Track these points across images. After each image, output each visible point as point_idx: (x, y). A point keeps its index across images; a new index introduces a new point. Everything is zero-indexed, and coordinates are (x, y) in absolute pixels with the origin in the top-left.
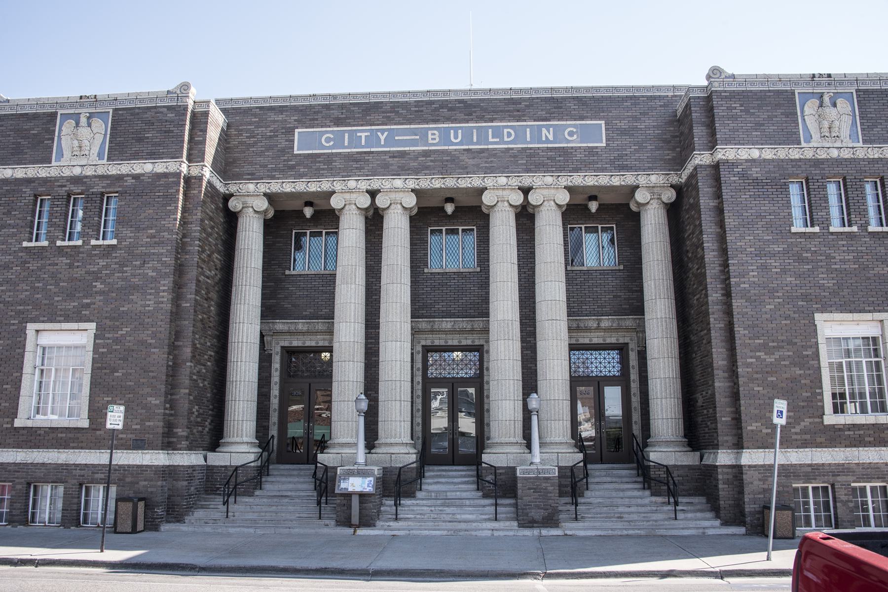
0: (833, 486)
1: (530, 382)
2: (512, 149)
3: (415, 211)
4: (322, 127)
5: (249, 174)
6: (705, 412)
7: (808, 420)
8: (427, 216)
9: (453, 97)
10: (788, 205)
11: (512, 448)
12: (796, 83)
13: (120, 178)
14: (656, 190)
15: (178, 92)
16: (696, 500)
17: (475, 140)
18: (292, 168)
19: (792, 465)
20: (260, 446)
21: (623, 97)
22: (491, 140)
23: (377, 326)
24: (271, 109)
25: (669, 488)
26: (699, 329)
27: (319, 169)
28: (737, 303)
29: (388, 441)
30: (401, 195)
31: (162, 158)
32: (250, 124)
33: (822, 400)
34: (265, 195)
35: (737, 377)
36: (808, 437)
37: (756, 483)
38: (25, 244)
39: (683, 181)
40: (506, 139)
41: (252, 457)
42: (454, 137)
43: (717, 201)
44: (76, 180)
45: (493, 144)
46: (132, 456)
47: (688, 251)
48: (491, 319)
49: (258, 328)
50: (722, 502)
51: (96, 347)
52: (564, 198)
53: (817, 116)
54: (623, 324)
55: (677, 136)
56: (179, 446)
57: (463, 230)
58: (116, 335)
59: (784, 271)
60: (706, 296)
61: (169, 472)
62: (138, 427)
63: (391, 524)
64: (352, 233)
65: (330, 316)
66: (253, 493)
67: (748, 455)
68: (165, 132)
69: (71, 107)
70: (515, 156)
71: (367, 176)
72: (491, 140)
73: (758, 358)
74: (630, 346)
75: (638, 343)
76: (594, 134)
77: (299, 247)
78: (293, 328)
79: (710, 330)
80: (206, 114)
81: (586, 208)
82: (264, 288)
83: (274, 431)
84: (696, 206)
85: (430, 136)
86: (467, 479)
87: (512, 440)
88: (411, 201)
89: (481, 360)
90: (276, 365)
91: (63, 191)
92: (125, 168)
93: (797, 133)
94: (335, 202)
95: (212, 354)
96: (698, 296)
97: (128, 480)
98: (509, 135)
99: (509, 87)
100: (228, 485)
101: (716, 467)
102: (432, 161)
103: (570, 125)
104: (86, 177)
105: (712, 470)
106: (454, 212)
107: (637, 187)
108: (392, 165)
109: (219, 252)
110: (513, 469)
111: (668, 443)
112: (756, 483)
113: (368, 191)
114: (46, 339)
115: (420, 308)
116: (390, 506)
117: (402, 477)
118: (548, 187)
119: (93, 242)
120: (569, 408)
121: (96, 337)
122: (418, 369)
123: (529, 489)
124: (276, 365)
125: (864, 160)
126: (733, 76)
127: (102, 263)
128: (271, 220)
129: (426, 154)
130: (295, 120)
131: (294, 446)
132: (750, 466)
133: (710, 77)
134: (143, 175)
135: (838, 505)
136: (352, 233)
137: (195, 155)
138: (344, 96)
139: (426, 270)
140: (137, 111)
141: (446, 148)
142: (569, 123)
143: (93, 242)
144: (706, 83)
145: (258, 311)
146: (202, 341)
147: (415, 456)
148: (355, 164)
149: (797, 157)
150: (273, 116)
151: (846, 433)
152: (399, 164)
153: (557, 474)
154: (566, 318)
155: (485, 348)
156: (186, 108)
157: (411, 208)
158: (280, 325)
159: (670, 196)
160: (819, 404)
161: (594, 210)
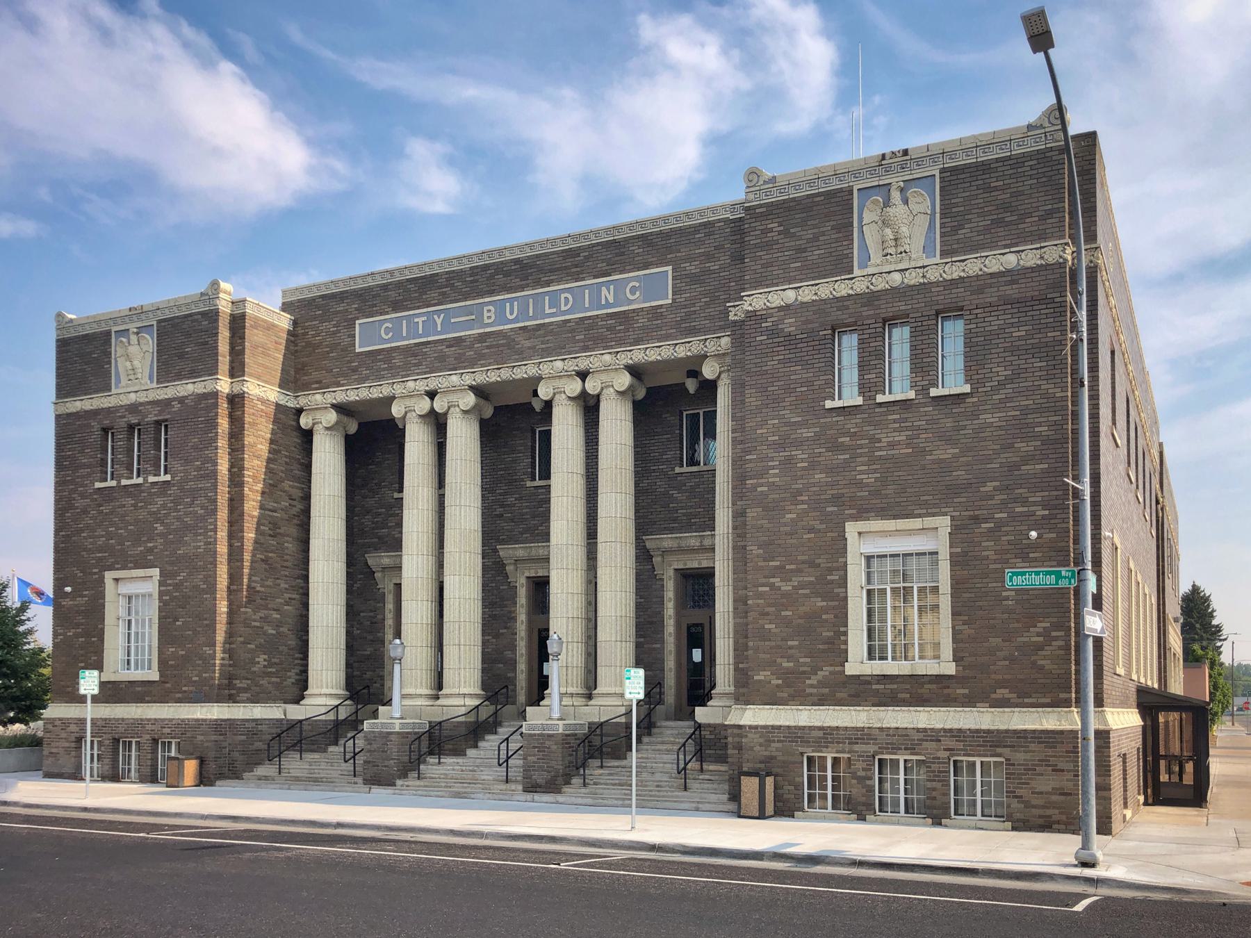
2: (569, 321)
4: (381, 314)
5: (317, 382)
9: (508, 256)
13: (167, 403)
18: (354, 370)
21: (694, 226)
22: (548, 311)
24: (333, 296)
34: (471, 388)
37: (757, 748)
38: (98, 485)
40: (563, 308)
42: (500, 313)
44: (134, 408)
45: (551, 316)
51: (161, 594)
59: (813, 465)
61: (220, 726)
69: (124, 323)
72: (548, 311)
73: (772, 586)
85: (486, 314)
91: (122, 423)
92: (972, 266)
94: (397, 410)
97: (188, 735)
102: (488, 347)
103: (632, 278)
104: (141, 404)
106: (697, 391)
112: (757, 748)
114: (125, 589)
119: (152, 479)
121: (161, 584)
125: (937, 284)
126: (773, 180)
127: (160, 501)
129: (482, 338)
132: (751, 727)
134: (186, 397)
141: (501, 328)
142: (631, 274)
143: (152, 479)
146: (269, 583)
148: (415, 359)
149: (844, 293)
158: (667, 541)
160: (843, 647)
161: (692, 391)
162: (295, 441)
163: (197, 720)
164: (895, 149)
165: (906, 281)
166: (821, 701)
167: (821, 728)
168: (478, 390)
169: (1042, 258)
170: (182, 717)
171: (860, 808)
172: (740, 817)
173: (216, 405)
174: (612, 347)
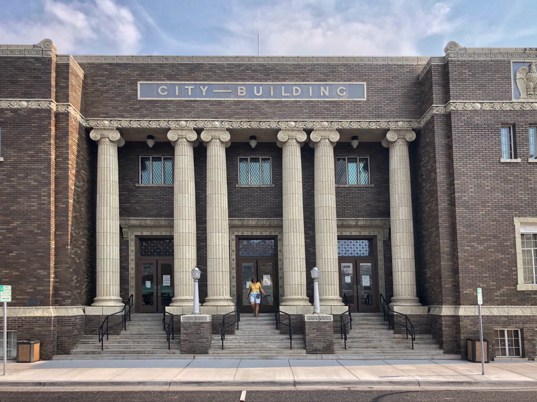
0: (522, 330)
1: (311, 261)
3: (229, 145)
4: (158, 80)
5: (104, 114)
6: (432, 281)
7: (506, 288)
8: (240, 149)
9: (255, 62)
10: (499, 143)
11: (300, 302)
12: (512, 54)
14: (401, 132)
15: (43, 47)
16: (425, 336)
17: (272, 94)
19: (494, 316)
20: (123, 302)
22: (284, 94)
23: (205, 222)
24: (118, 65)
25: (407, 329)
26: (430, 227)
27: (157, 112)
28: (459, 210)
29: (215, 297)
30: (219, 133)
31: (34, 98)
32: (103, 76)
33: (516, 275)
34: (118, 129)
35: (457, 259)
36: (506, 298)
37: (469, 327)
39: (421, 126)
40: (294, 94)
41: (118, 310)
42: (258, 92)
43: (448, 140)
46: (28, 310)
47: (422, 175)
48: (392, 218)
49: (118, 223)
50: (444, 339)
52: (336, 137)
53: (525, 79)
54: (272, 223)
55: (418, 94)
56: (64, 303)
57: (263, 159)
58: (9, 227)
60: (437, 205)
62: (32, 290)
63: (219, 352)
64: (185, 158)
65: (171, 214)
66: (120, 332)
67: (463, 309)
68: (35, 77)
70: (301, 107)
71: (194, 118)
73: (472, 247)
74: (378, 238)
75: (384, 235)
76: (356, 92)
77: (144, 168)
78: (143, 223)
79: (438, 227)
80: (67, 66)
81: (349, 145)
82: (120, 195)
83: (132, 292)
84: (432, 144)
85: (239, 91)
86: (266, 318)
87: (300, 297)
88: (227, 137)
89: (276, 245)
90: (132, 247)
93: (509, 92)
94: (171, 136)
95: (85, 240)
96: (430, 205)
98: (297, 91)
99: (297, 55)
100: (104, 328)
101: (441, 316)
102: (241, 109)
105: (438, 318)
106: (256, 146)
107: (388, 130)
108: (212, 110)
109: (85, 170)
110: (302, 317)
111: (405, 300)
112: (469, 327)
113: (195, 129)
115: (234, 210)
116: (218, 340)
117: (226, 321)
118: (324, 129)
120: (338, 277)
122: (233, 251)
123: (314, 329)
124: (132, 247)
128: (122, 148)
129: (237, 103)
130: (137, 75)
131: (150, 294)
132: (465, 316)
133: (448, 49)
134: (19, 109)
135: (525, 342)
136: (185, 158)
137: (63, 96)
138: (174, 58)
139: (237, 186)
140: (9, 59)
141: (251, 99)
144: (444, 54)
145: (118, 211)
147: (233, 307)
148: (184, 109)
149: (508, 109)
150: (120, 71)
151: (532, 296)
152: (217, 110)
153: (332, 320)
154: (335, 218)
155: (279, 237)
156: (50, 60)
157: (226, 142)
158: (134, 221)
159: (412, 136)
160: (514, 277)
161: (355, 146)
162: (91, 149)
163: (36, 317)
164: (532, 47)
165: (29, 106)
166: (503, 303)
167: (506, 316)
168: (121, 130)
169: (39, 105)
170: (19, 315)
171: (529, 354)
172: (18, 362)
173: (50, 118)
174: (328, 118)
